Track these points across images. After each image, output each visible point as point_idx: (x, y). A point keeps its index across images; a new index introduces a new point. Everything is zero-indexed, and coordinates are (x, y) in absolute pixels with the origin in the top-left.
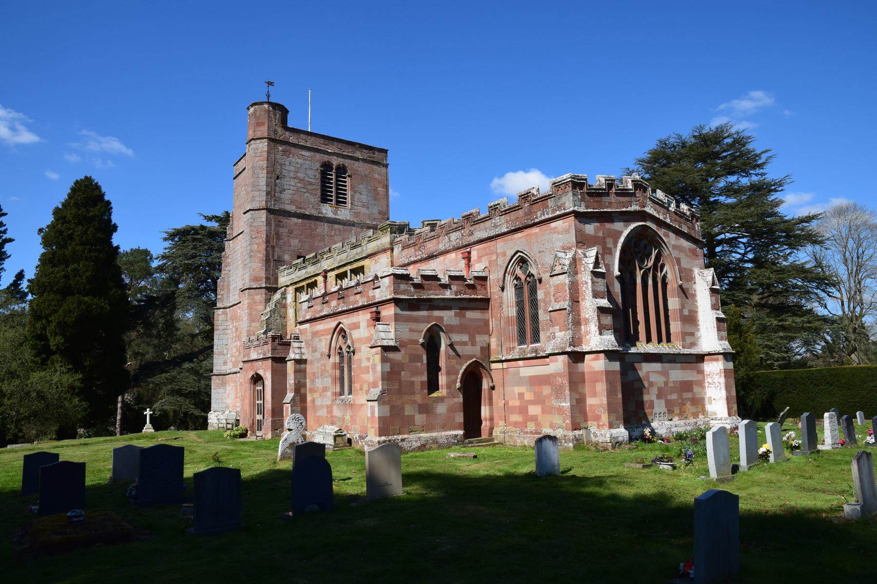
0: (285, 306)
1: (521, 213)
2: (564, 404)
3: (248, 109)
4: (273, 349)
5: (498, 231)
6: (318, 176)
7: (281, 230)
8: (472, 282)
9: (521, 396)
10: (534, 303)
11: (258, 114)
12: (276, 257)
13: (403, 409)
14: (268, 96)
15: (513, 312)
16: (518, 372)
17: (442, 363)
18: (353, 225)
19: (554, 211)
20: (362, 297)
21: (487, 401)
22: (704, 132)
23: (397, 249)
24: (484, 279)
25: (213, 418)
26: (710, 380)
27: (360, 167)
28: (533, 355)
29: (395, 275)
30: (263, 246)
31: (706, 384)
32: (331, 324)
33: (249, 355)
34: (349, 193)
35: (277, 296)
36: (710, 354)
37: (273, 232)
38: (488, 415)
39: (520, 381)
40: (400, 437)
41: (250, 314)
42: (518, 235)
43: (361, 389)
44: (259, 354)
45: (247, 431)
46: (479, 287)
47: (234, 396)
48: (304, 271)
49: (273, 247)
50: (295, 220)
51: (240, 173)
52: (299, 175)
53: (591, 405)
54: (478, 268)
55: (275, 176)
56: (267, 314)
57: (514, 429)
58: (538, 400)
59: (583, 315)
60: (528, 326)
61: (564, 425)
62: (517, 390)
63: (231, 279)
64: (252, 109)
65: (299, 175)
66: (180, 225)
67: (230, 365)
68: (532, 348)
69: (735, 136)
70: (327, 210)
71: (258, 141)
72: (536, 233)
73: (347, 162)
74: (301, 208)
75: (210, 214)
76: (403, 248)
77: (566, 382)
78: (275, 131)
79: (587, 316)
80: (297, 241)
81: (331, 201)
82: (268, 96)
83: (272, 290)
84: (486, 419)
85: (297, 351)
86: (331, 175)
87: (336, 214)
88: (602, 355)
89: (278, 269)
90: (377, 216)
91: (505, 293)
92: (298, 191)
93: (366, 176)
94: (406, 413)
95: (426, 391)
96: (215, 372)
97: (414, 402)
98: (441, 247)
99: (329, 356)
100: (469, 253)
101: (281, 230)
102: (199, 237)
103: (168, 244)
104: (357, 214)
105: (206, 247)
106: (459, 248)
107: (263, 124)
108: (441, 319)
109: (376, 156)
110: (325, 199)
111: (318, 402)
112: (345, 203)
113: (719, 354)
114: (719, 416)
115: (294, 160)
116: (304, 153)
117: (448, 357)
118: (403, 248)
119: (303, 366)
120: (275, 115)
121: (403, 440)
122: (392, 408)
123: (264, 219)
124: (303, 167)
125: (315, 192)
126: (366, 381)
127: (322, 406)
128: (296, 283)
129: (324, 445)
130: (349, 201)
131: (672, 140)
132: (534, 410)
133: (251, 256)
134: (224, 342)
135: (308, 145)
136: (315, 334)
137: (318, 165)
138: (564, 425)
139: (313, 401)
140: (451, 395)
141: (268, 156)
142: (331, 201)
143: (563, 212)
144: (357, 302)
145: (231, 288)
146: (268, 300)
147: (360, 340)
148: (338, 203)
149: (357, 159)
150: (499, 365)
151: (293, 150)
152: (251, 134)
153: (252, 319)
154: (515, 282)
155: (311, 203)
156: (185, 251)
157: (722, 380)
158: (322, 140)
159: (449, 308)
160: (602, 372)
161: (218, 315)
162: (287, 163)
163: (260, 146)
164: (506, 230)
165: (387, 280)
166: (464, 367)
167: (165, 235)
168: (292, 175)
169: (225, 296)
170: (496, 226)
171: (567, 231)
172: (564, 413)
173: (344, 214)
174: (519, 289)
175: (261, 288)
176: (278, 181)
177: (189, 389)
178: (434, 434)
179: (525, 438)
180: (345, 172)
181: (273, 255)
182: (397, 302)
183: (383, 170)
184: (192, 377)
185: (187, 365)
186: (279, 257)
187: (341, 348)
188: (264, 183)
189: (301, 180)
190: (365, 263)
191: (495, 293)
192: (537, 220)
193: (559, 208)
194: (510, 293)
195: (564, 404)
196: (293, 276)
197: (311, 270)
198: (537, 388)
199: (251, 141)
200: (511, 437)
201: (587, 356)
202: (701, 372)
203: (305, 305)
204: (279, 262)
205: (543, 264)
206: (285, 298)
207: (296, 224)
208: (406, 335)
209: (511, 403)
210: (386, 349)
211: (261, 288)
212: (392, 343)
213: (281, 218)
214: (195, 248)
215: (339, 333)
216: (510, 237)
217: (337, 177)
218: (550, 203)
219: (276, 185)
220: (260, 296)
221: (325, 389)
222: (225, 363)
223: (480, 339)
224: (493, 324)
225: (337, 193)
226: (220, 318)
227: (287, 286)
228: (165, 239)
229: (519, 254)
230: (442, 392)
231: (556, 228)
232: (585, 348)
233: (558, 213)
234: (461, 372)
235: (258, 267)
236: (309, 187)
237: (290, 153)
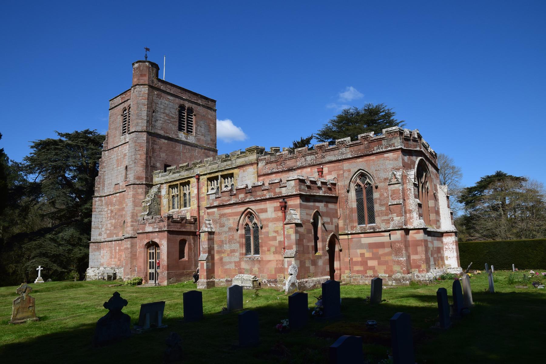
0: (160, 197)
1: (362, 147)
2: (402, 259)
3: (133, 64)
4: (168, 225)
5: (344, 157)
6: (177, 113)
7: (155, 146)
8: (330, 186)
9: (362, 255)
10: (371, 200)
11: (141, 68)
12: (152, 164)
13: (305, 262)
14: (146, 58)
15: (354, 205)
16: (360, 241)
17: (319, 235)
18: (197, 147)
19: (386, 147)
20: (269, 192)
21: (338, 258)
22: (371, 108)
23: (261, 165)
24: (334, 185)
25: (91, 273)
26: (447, 247)
27: (200, 110)
28: (372, 230)
29: (299, 179)
30: (144, 156)
31: (445, 249)
32: (242, 209)
33: (144, 228)
34: (194, 126)
35: (154, 190)
36: (447, 232)
37: (150, 148)
38: (338, 266)
39: (362, 246)
40: (305, 280)
41: (134, 202)
42: (360, 160)
43: (269, 250)
44: (154, 228)
45: (142, 280)
46: (333, 190)
47: (108, 257)
48: (177, 175)
49: (150, 157)
50: (163, 141)
51: (116, 106)
52: (166, 111)
53: (414, 260)
54: (329, 178)
55: (152, 110)
56: (148, 202)
57: (357, 275)
58: (375, 257)
59: (408, 208)
60: (366, 212)
61: (402, 271)
62: (359, 251)
63: (106, 177)
64: (136, 65)
65: (166, 111)
66: (44, 138)
67: (105, 236)
68: (370, 227)
69: (387, 112)
70: (182, 136)
71: (142, 86)
72: (373, 160)
73: (194, 106)
74: (167, 133)
75: (64, 132)
76: (267, 163)
77: (402, 246)
78: (153, 81)
79: (411, 208)
80: (164, 154)
81: (184, 130)
82: (146, 58)
83: (149, 186)
84: (337, 269)
85: (209, 226)
86: (184, 113)
87: (187, 139)
88: (422, 231)
89: (153, 172)
90: (210, 142)
91: (350, 194)
92: (166, 123)
93: (204, 116)
94: (307, 265)
95: (314, 252)
96: (92, 240)
97: (309, 258)
98: (299, 164)
99: (237, 230)
100: (322, 168)
101: (155, 146)
102: (59, 147)
103: (32, 151)
104: (199, 140)
105: (65, 155)
106: (314, 165)
107: (145, 75)
108: (318, 207)
109: (209, 104)
110: (181, 129)
111: (226, 259)
112: (192, 132)
113: (452, 232)
114: (452, 267)
115: (163, 101)
116: (169, 97)
117: (322, 231)
118: (267, 163)
119: (212, 236)
120: (153, 71)
121: (306, 282)
122: (301, 262)
123: (145, 138)
124: (168, 106)
125: (175, 123)
126: (273, 246)
127: (230, 262)
128: (170, 182)
129: (242, 287)
130: (194, 131)
131: (351, 111)
132: (371, 263)
133: (135, 163)
134: (100, 220)
135: (172, 92)
136: (222, 216)
137: (177, 106)
138: (402, 271)
139: (221, 259)
140: (324, 255)
141: (148, 97)
142: (184, 130)
143: (393, 148)
144: (265, 195)
145: (106, 183)
146: (147, 193)
147: (268, 220)
148: (188, 131)
149: (199, 105)
150: (346, 237)
151: (163, 94)
152: (135, 81)
153: (135, 204)
154: (356, 187)
155: (172, 130)
156: (49, 156)
157: (454, 247)
158: (179, 90)
159: (321, 202)
160: (421, 240)
161: (96, 201)
162: (159, 103)
163: (143, 89)
164: (351, 156)
165: (293, 183)
166: (329, 237)
167: (33, 144)
168: (162, 110)
169: (101, 189)
170: (342, 154)
171: (396, 159)
172: (401, 264)
173: (191, 139)
174: (359, 191)
175: (142, 184)
176: (154, 114)
177: (53, 253)
178: (319, 278)
179: (366, 280)
180: (192, 112)
181: (150, 162)
182: (301, 196)
183: (214, 113)
184: (53, 244)
185: (49, 236)
186: (154, 164)
187: (247, 224)
188: (145, 114)
189: (167, 115)
190: (235, 171)
191: (341, 194)
192: (374, 152)
193: (390, 146)
194: (353, 194)
195: (402, 259)
196: (167, 177)
197: (184, 174)
198: (374, 250)
199: (136, 85)
200: (355, 279)
201: (411, 232)
202: (442, 242)
203: (213, 197)
204: (154, 168)
205: (378, 178)
206: (160, 192)
207: (164, 143)
208: (305, 217)
209: (354, 259)
210: (298, 225)
211: (142, 184)
212: (299, 222)
213: (155, 138)
214: (56, 154)
215: (246, 215)
216: (353, 161)
217: (188, 115)
218: (384, 142)
219: (152, 116)
220: (141, 190)
221: (233, 251)
222: (100, 234)
223: (335, 220)
224: (340, 212)
225: (188, 126)
226: (97, 203)
227: (162, 184)
228: (32, 147)
229: (361, 171)
230: (319, 253)
231: (388, 157)
232: (409, 227)
233: (389, 149)
234: (328, 240)
235: (138, 170)
236: (172, 120)
237: (161, 97)
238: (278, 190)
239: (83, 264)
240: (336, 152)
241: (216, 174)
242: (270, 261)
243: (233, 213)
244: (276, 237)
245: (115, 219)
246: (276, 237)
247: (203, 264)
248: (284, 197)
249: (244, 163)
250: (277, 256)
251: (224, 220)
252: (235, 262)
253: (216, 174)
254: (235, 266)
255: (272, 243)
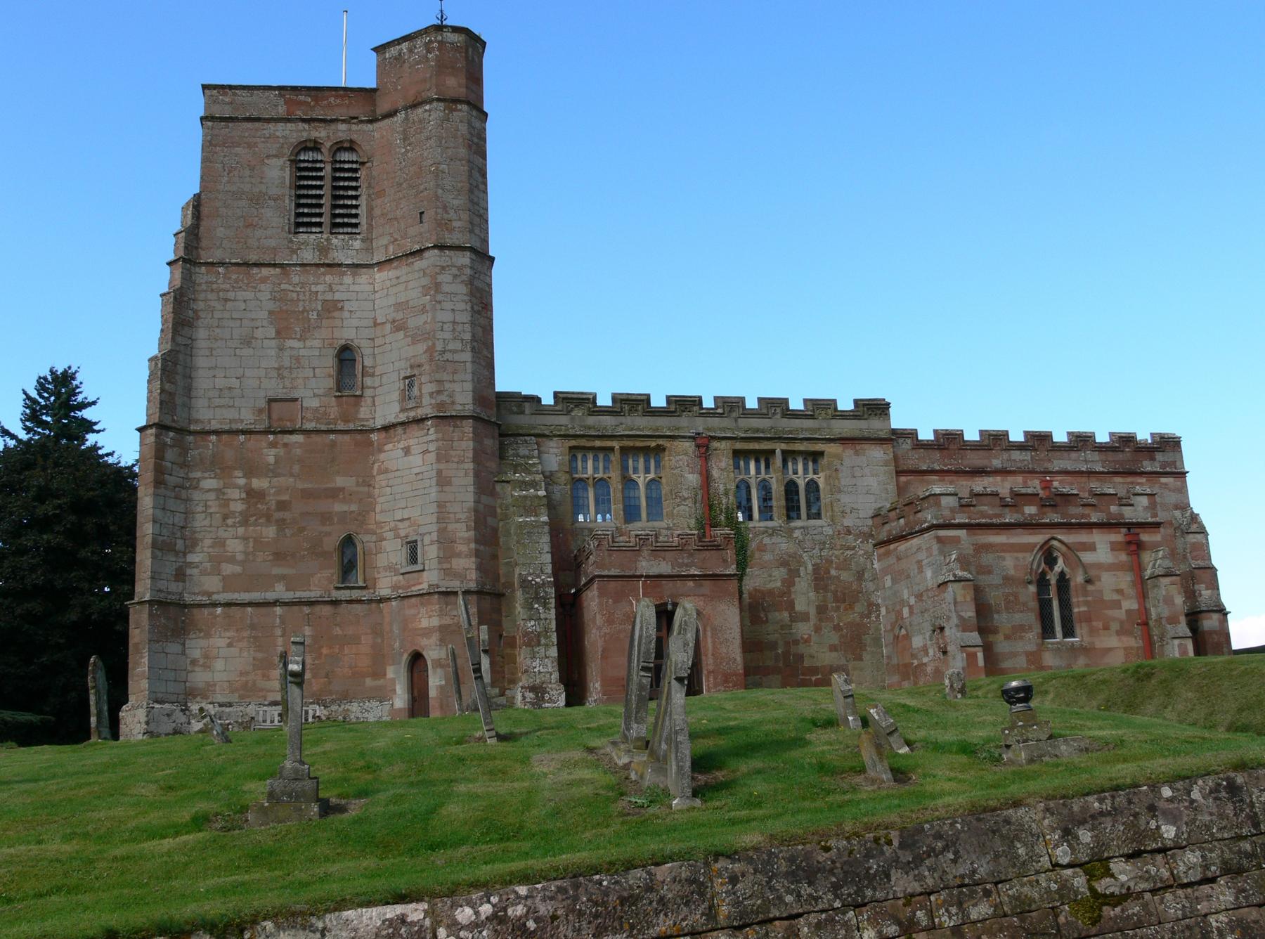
32: (1038, 538)
43: (1106, 628)
106: (1032, 472)
128: (575, 436)
136: (980, 549)
190: (830, 449)
238: (1113, 509)
239: (385, 675)
240: (1074, 455)
241: (608, 444)
242: (1110, 649)
243: (1012, 545)
244: (1119, 602)
245: (281, 524)
246: (1119, 602)
247: (975, 655)
248: (1129, 525)
249: (857, 434)
250: (1124, 638)
251: (987, 559)
252: (1028, 654)
253: (608, 444)
254: (1028, 661)
255: (1110, 613)
